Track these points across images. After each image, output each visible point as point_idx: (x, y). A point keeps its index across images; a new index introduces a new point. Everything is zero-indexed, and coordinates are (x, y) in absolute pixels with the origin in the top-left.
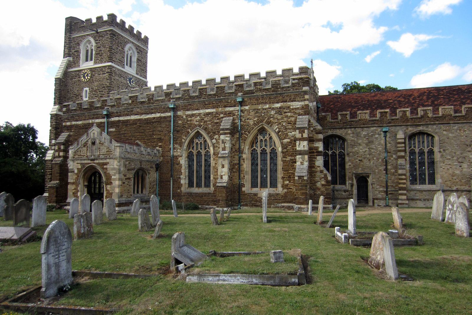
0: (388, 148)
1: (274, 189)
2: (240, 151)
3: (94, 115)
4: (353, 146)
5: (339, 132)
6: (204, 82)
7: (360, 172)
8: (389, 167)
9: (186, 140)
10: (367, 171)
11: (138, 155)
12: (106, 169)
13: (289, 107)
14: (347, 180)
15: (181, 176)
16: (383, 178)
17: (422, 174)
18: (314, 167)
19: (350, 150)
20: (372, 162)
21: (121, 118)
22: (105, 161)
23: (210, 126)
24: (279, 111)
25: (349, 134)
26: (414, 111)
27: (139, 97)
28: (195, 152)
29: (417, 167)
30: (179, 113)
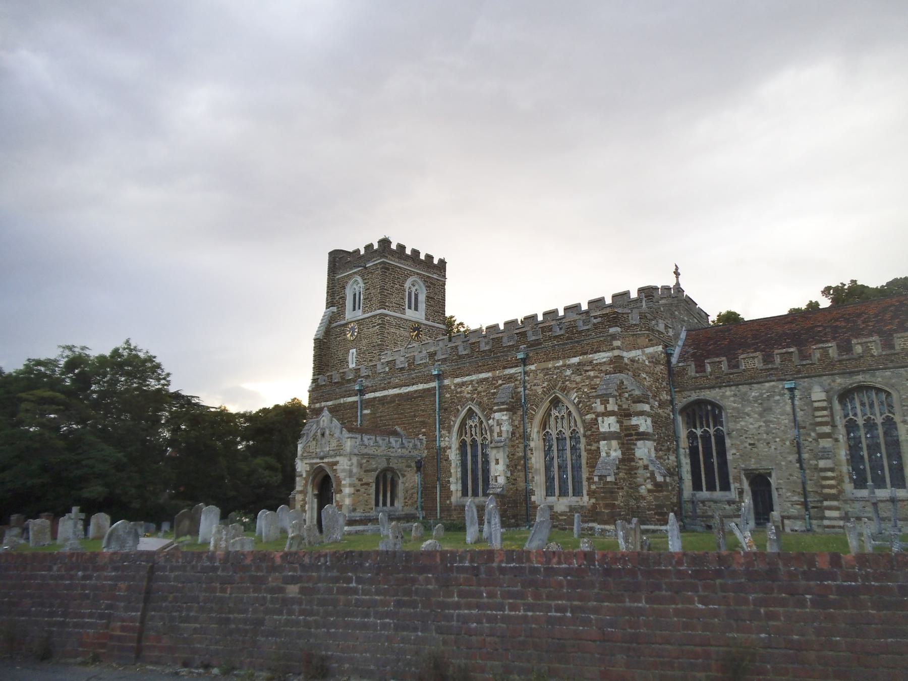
0: (798, 418)
1: (578, 499)
2: (526, 437)
3: (346, 391)
4: (736, 419)
5: (708, 395)
6: (608, 301)
7: (753, 467)
8: (805, 456)
9: (455, 422)
10: (766, 465)
11: (383, 448)
12: (336, 470)
13: (591, 362)
14: (731, 481)
15: (451, 479)
16: (797, 476)
17: (876, 466)
18: (633, 460)
19: (732, 425)
20: (773, 447)
21: (378, 394)
23: (485, 399)
24: (578, 369)
25: (728, 397)
26: (845, 348)
27: (417, 358)
28: (468, 440)
29: (865, 453)
30: (446, 382)
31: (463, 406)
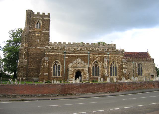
17: (140, 73)
21: (70, 54)
22: (83, 68)
24: (118, 57)
28: (112, 67)
30: (91, 55)
31: (95, 60)
